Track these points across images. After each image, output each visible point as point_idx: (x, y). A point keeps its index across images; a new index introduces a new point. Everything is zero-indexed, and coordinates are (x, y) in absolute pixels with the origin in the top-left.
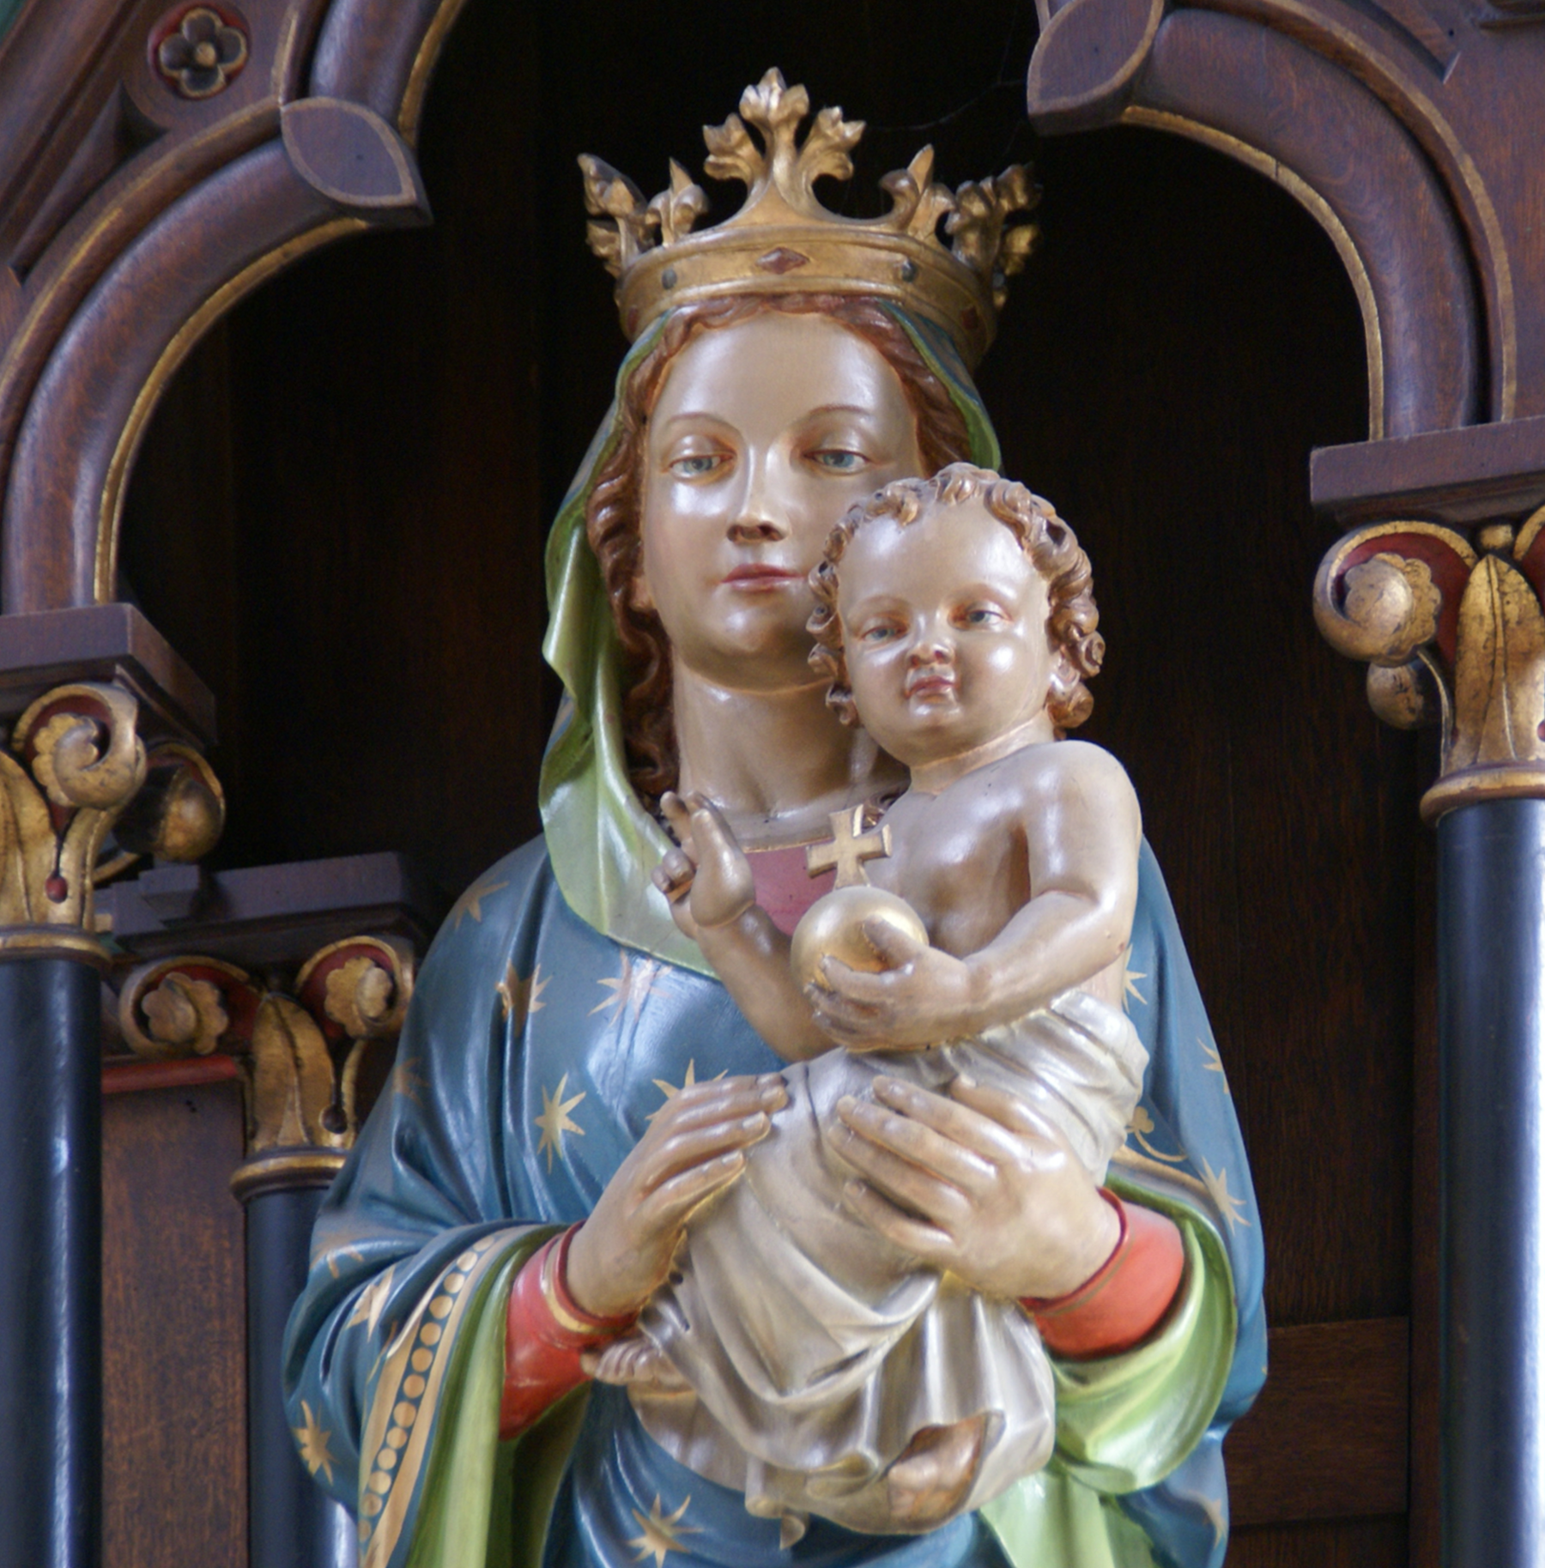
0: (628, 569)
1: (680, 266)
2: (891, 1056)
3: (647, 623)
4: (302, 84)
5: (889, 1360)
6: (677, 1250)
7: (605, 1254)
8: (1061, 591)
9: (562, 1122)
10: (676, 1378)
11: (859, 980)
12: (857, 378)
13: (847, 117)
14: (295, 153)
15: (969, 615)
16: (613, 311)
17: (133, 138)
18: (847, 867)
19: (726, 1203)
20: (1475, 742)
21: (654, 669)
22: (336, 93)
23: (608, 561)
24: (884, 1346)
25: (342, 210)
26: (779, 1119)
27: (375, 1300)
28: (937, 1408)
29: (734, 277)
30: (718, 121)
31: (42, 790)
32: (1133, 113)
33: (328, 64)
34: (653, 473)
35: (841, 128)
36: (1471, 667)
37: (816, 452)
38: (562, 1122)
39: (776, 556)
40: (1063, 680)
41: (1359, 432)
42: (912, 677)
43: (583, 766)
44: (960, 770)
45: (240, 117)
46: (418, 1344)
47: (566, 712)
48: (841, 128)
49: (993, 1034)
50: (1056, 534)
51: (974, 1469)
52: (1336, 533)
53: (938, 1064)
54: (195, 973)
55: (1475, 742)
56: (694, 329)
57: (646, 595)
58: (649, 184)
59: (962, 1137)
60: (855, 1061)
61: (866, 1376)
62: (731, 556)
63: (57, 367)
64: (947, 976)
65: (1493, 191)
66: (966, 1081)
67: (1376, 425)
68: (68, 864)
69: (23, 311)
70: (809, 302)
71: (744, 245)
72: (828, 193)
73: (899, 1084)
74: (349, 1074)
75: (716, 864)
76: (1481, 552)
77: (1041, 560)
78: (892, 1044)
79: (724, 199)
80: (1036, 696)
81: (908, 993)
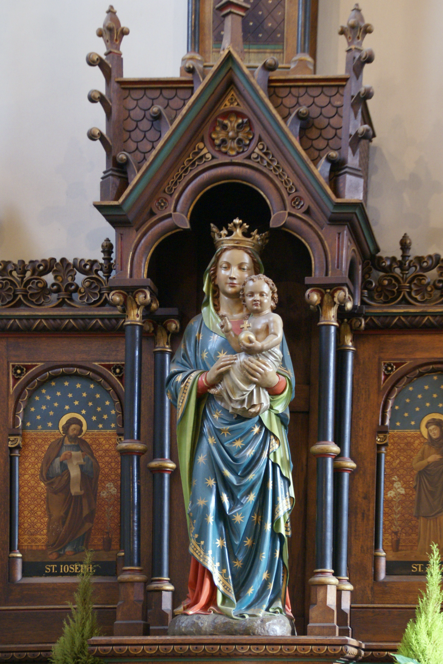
1: (224, 241)
4: (175, 210)
5: (249, 396)
6: (221, 377)
7: (211, 375)
8: (273, 293)
9: (205, 355)
12: (246, 259)
13: (247, 225)
14: (174, 220)
16: (214, 245)
17: (152, 214)
18: (246, 328)
20: (325, 317)
21: (217, 293)
22: (179, 212)
24: (248, 393)
25: (179, 228)
26: (236, 361)
27: (179, 378)
28: (255, 402)
30: (230, 223)
31: (136, 303)
33: (179, 208)
34: (219, 269)
38: (205, 355)
39: (235, 282)
40: (273, 304)
41: (311, 275)
42: (254, 303)
44: (259, 316)
46: (186, 385)
47: (205, 298)
50: (273, 285)
54: (150, 321)
56: (225, 250)
57: (217, 283)
58: (221, 229)
61: (246, 397)
62: (229, 281)
63: (140, 245)
65: (329, 245)
66: (260, 359)
67: (313, 274)
68: (139, 312)
69: (136, 237)
72: (244, 234)
74: (169, 337)
75: (227, 325)
77: (271, 289)
78: (251, 351)
79: (230, 233)
80: (269, 306)
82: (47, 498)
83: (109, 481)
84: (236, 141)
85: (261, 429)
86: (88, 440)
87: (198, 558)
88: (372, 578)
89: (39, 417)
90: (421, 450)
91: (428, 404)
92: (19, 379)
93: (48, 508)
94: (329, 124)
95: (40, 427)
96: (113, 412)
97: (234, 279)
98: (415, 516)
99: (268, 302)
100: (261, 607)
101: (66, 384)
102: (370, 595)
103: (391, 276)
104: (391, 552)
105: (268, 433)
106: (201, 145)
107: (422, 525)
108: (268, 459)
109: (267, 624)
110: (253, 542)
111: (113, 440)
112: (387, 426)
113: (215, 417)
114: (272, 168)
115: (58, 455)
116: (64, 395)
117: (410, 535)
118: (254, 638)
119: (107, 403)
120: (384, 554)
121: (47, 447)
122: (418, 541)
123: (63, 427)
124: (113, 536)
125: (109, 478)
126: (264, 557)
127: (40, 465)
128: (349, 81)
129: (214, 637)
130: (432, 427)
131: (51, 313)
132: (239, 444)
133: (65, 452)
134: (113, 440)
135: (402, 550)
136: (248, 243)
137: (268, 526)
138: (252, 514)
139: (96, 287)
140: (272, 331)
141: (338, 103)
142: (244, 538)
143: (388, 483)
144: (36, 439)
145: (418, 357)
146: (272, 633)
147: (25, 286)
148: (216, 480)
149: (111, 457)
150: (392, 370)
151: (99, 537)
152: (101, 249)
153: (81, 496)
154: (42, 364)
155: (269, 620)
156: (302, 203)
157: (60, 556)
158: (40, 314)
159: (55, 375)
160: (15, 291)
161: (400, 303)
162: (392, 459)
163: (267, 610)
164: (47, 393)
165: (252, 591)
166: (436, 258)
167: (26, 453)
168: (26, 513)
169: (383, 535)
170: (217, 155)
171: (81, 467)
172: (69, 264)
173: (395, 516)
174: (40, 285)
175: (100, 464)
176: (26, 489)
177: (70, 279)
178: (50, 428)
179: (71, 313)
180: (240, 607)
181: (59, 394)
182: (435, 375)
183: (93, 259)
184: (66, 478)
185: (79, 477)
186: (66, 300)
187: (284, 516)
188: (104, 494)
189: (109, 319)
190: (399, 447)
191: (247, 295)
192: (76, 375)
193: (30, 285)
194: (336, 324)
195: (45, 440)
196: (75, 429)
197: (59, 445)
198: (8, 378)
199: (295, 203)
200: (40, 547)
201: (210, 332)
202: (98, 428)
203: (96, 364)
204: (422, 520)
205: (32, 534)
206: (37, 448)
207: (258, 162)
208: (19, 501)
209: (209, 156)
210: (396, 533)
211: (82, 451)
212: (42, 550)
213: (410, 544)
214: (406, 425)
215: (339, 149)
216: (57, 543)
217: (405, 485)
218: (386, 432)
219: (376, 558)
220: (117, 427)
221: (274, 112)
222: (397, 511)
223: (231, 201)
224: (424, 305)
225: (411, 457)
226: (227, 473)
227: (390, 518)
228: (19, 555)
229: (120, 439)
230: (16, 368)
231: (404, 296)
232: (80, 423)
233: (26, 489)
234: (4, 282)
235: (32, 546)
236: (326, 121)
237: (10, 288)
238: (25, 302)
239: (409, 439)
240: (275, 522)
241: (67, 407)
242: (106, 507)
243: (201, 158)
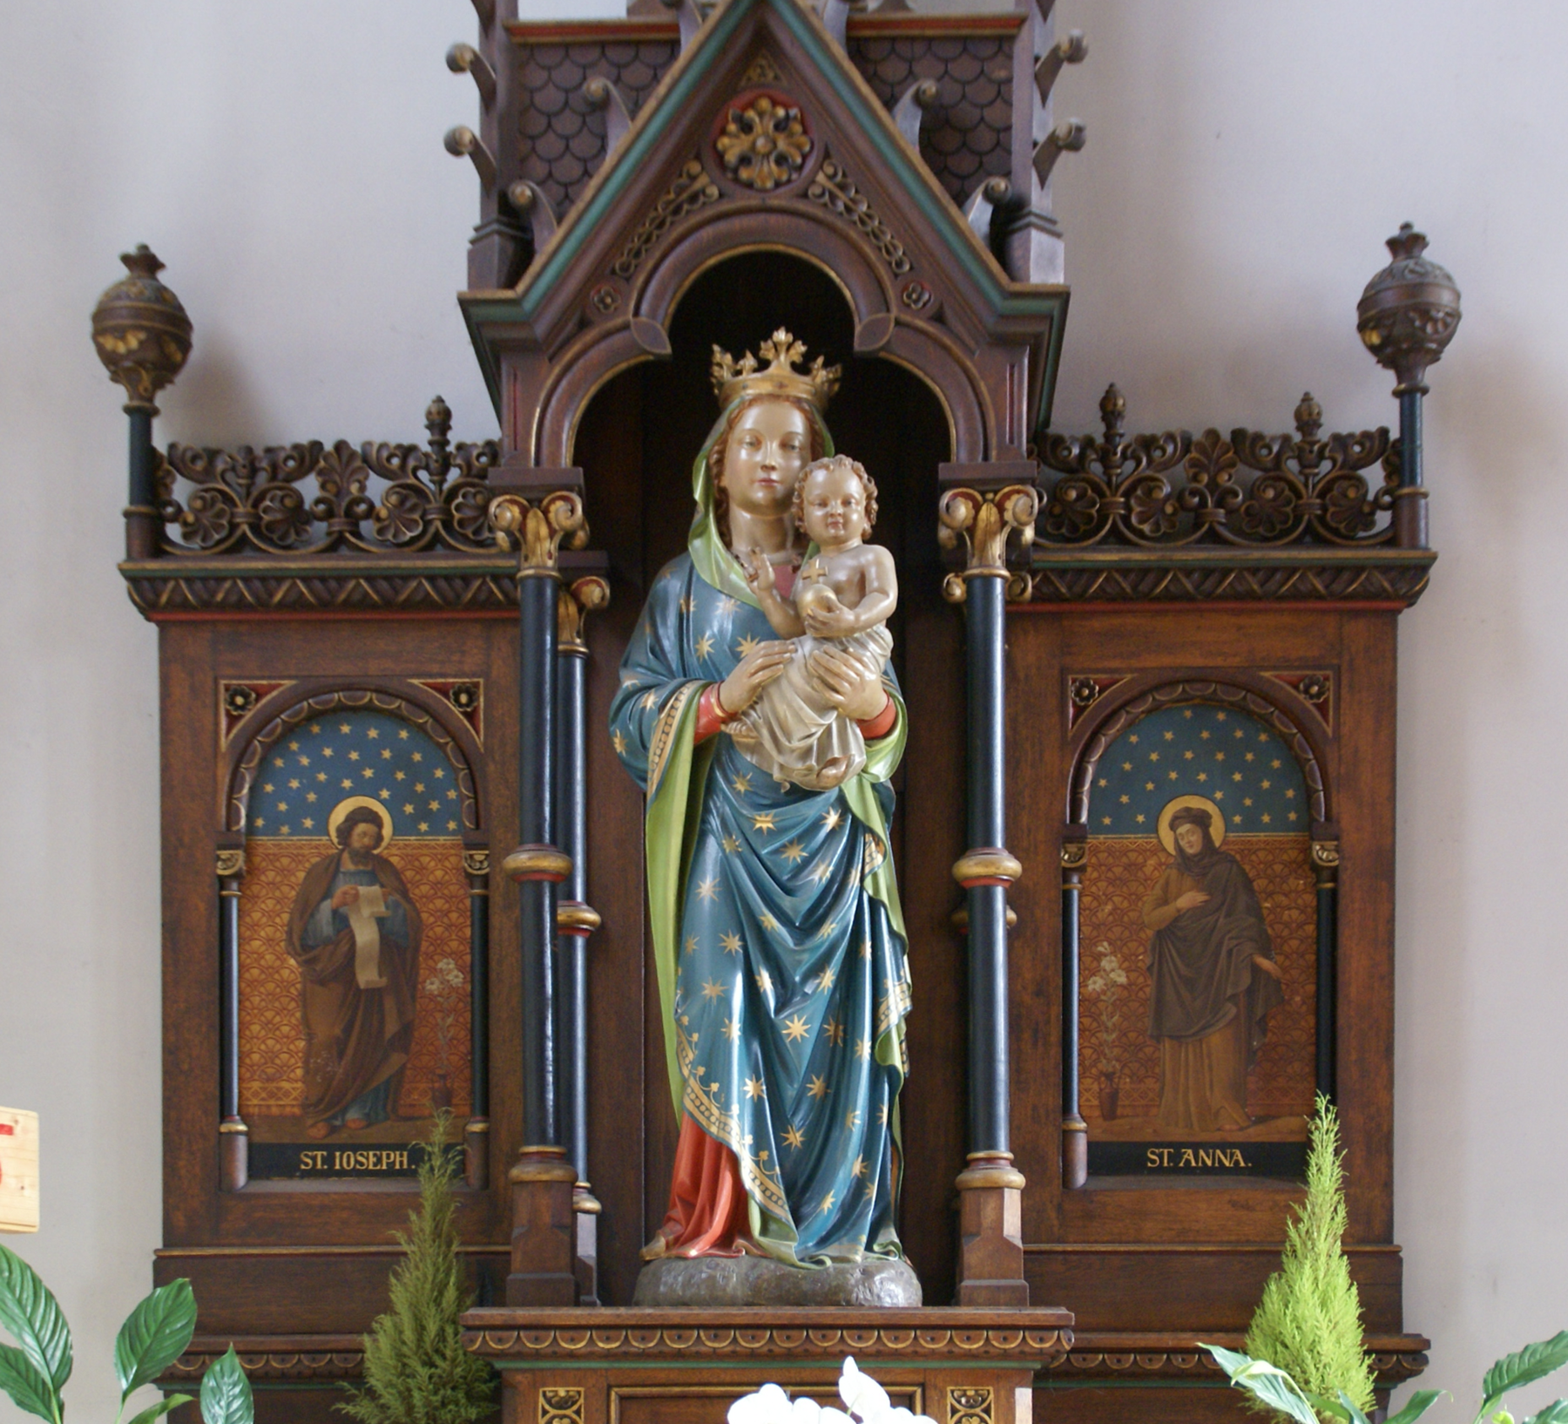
0: (719, 475)
2: (827, 639)
3: (723, 492)
4: (637, 313)
6: (758, 695)
7: (733, 689)
8: (869, 497)
10: (754, 734)
11: (822, 614)
15: (846, 503)
17: (584, 324)
19: (776, 680)
23: (715, 471)
27: (650, 700)
29: (766, 388)
32: (882, 354)
33: (645, 307)
35: (800, 348)
36: (979, 534)
37: (786, 445)
39: (774, 476)
40: (867, 526)
41: (947, 459)
43: (703, 531)
45: (619, 321)
46: (669, 715)
47: (698, 517)
48: (800, 348)
49: (857, 635)
51: (845, 772)
52: (944, 490)
53: (841, 643)
55: (981, 559)
58: (738, 357)
59: (852, 667)
60: (815, 639)
61: (814, 741)
62: (761, 474)
64: (849, 616)
67: (954, 458)
69: (550, 371)
70: (787, 398)
71: (770, 379)
72: (795, 367)
73: (828, 647)
76: (985, 501)
77: (865, 488)
79: (763, 365)
81: (838, 620)
82: (303, 994)
83: (444, 955)
84: (772, 158)
85: (842, 817)
86: (394, 860)
87: (704, 1123)
88: (1058, 1182)
89: (283, 807)
90: (1162, 881)
91: (1173, 775)
92: (240, 717)
93: (306, 1020)
94: (982, 119)
95: (285, 829)
96: (452, 794)
97: (773, 468)
98: (1151, 1036)
99: (859, 520)
100: (855, 1240)
101: (346, 729)
102: (1055, 1222)
103: (1083, 480)
104: (1100, 1120)
105: (860, 828)
106: (695, 167)
107: (1167, 1057)
108: (862, 888)
109: (877, 1278)
110: (828, 1087)
111: (452, 859)
112: (1083, 826)
113: (732, 789)
114: (856, 218)
115: (327, 894)
116: (341, 755)
117: (1141, 1081)
118: (852, 1315)
119: (439, 773)
120: (1083, 1125)
121: (301, 875)
122: (1160, 1096)
123: (339, 830)
124: (456, 1085)
125: (446, 948)
126: (858, 1122)
127: (286, 917)
128: (1026, 28)
129: (756, 1310)
130: (1184, 829)
131: (318, 564)
132: (796, 854)
133: (342, 888)
134: (452, 859)
135: (1123, 1116)
136: (802, 387)
137: (865, 1048)
138: (825, 1020)
139: (413, 509)
140: (876, 584)
141: (1002, 74)
142: (807, 1079)
143: (1088, 960)
144: (277, 857)
145: (1148, 664)
146: (887, 1302)
147: (255, 505)
148: (743, 938)
149: (448, 899)
150: (1091, 694)
151: (422, 1086)
152: (425, 422)
153: (379, 989)
154: (294, 682)
155: (880, 1270)
156: (926, 297)
157: (333, 1130)
158: (293, 565)
159: (320, 712)
160: (233, 515)
161: (1103, 541)
162: (1095, 904)
163: (869, 1248)
164: (302, 751)
165: (830, 1203)
166: (1183, 439)
167: (255, 889)
168: (255, 1028)
169: (1080, 1082)
170: (730, 187)
171: (380, 921)
172: (353, 454)
173: (1105, 1036)
174: (288, 502)
175: (424, 916)
176: (255, 972)
177: (354, 488)
178: (307, 832)
179: (362, 564)
180: (806, 1242)
181: (328, 752)
182: (1188, 708)
183: (406, 442)
184: (346, 948)
185: (377, 947)
186: (348, 535)
187: (898, 1026)
188: (433, 986)
189: (448, 578)
190: (1110, 875)
191: (812, 504)
192: (369, 709)
193: (268, 503)
194: (1005, 573)
195: (297, 859)
196: (365, 834)
197: (327, 873)
198: (216, 715)
199: (909, 297)
200: (288, 1109)
201: (712, 592)
202: (419, 833)
203: (416, 681)
204: (1167, 1044)
205: (270, 1079)
206: (278, 879)
207: (825, 205)
208: (240, 1002)
209: (713, 191)
210: (1109, 1076)
211: (382, 886)
212: (294, 1116)
213: (1143, 1102)
214: (1123, 824)
215: (1007, 174)
216: (328, 1100)
217: (1126, 964)
218: (1082, 839)
219: (1067, 1136)
220: (462, 828)
221: (865, 89)
222: (1110, 1024)
223: (754, 297)
224: (1158, 545)
225: (1139, 898)
226: (770, 921)
227: (1093, 1040)
228: (242, 1128)
229: (471, 856)
230: (233, 692)
231: (1114, 523)
232: (375, 819)
233: (255, 972)
234: (208, 496)
235: (268, 1107)
236: (977, 113)
237: (223, 510)
238: (255, 541)
239: (1132, 856)
240: (879, 1039)
241: (347, 784)
242: (438, 1016)
243: (693, 198)
